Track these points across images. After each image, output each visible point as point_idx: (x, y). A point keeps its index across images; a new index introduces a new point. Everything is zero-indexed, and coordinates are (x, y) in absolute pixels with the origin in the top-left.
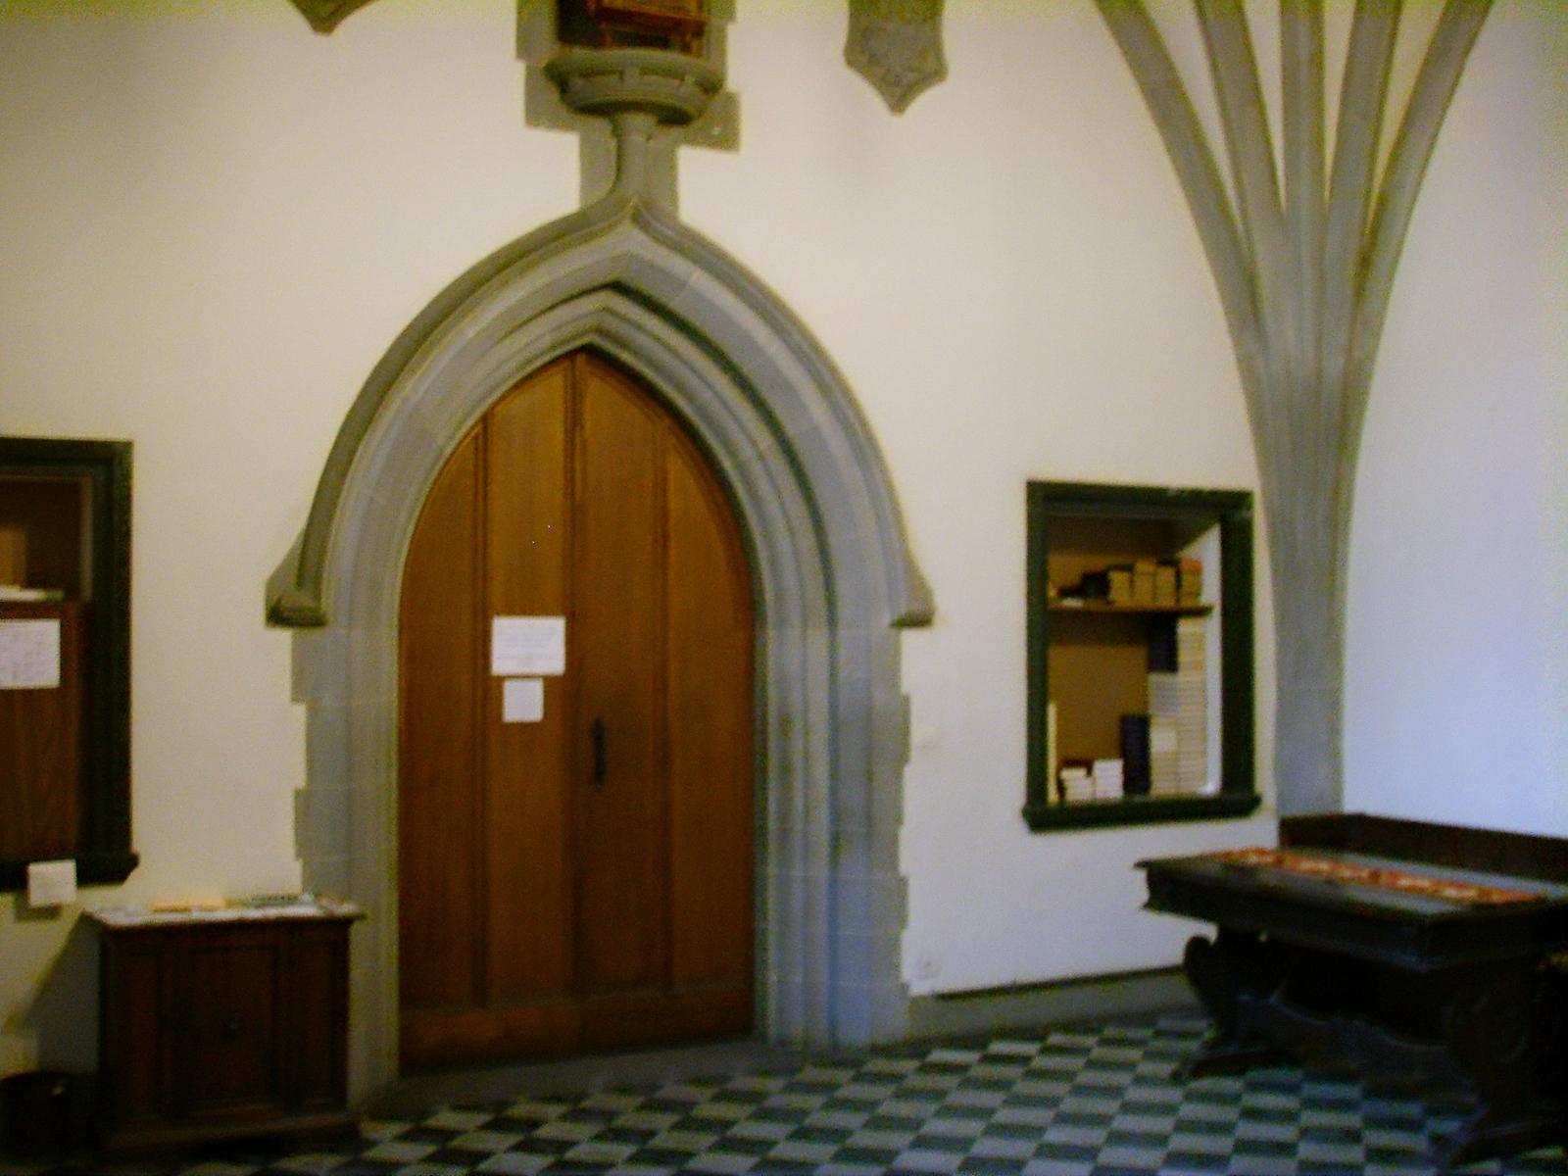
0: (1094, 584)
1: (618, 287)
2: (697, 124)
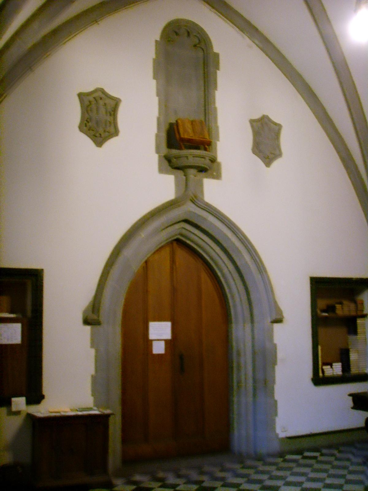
0: (331, 309)
1: (186, 221)
2: (209, 172)
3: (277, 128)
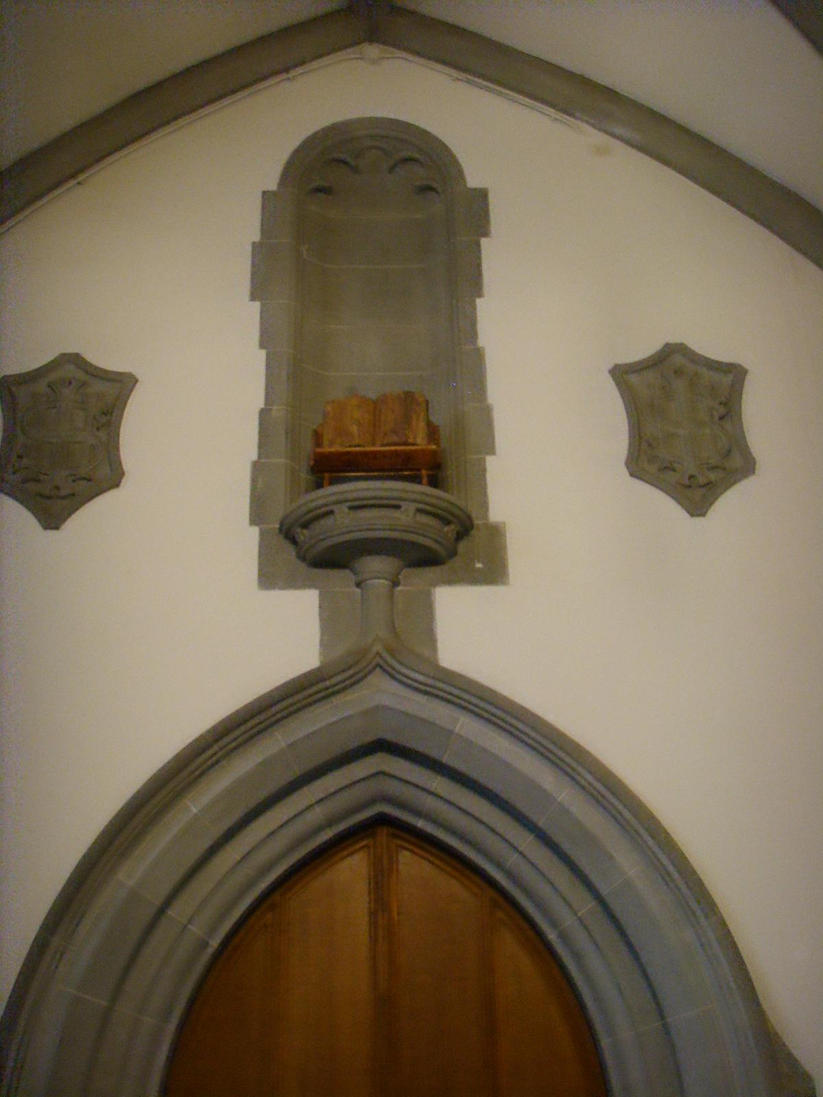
3: (727, 379)
